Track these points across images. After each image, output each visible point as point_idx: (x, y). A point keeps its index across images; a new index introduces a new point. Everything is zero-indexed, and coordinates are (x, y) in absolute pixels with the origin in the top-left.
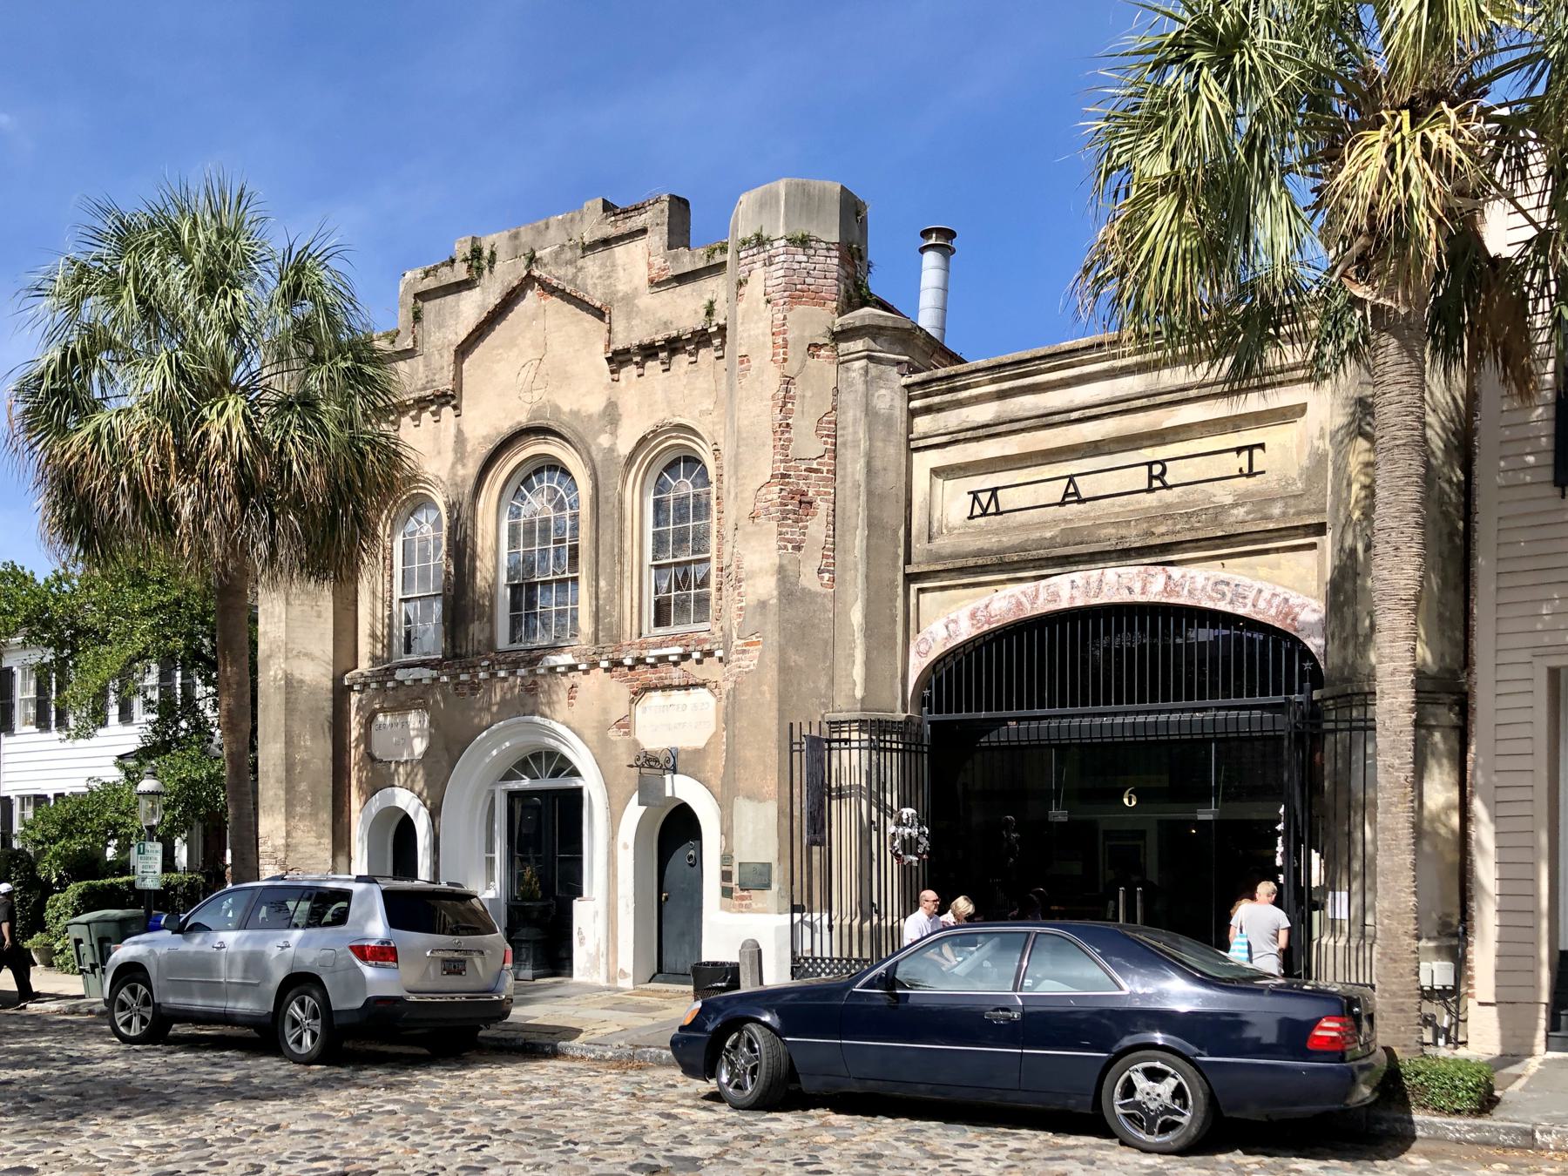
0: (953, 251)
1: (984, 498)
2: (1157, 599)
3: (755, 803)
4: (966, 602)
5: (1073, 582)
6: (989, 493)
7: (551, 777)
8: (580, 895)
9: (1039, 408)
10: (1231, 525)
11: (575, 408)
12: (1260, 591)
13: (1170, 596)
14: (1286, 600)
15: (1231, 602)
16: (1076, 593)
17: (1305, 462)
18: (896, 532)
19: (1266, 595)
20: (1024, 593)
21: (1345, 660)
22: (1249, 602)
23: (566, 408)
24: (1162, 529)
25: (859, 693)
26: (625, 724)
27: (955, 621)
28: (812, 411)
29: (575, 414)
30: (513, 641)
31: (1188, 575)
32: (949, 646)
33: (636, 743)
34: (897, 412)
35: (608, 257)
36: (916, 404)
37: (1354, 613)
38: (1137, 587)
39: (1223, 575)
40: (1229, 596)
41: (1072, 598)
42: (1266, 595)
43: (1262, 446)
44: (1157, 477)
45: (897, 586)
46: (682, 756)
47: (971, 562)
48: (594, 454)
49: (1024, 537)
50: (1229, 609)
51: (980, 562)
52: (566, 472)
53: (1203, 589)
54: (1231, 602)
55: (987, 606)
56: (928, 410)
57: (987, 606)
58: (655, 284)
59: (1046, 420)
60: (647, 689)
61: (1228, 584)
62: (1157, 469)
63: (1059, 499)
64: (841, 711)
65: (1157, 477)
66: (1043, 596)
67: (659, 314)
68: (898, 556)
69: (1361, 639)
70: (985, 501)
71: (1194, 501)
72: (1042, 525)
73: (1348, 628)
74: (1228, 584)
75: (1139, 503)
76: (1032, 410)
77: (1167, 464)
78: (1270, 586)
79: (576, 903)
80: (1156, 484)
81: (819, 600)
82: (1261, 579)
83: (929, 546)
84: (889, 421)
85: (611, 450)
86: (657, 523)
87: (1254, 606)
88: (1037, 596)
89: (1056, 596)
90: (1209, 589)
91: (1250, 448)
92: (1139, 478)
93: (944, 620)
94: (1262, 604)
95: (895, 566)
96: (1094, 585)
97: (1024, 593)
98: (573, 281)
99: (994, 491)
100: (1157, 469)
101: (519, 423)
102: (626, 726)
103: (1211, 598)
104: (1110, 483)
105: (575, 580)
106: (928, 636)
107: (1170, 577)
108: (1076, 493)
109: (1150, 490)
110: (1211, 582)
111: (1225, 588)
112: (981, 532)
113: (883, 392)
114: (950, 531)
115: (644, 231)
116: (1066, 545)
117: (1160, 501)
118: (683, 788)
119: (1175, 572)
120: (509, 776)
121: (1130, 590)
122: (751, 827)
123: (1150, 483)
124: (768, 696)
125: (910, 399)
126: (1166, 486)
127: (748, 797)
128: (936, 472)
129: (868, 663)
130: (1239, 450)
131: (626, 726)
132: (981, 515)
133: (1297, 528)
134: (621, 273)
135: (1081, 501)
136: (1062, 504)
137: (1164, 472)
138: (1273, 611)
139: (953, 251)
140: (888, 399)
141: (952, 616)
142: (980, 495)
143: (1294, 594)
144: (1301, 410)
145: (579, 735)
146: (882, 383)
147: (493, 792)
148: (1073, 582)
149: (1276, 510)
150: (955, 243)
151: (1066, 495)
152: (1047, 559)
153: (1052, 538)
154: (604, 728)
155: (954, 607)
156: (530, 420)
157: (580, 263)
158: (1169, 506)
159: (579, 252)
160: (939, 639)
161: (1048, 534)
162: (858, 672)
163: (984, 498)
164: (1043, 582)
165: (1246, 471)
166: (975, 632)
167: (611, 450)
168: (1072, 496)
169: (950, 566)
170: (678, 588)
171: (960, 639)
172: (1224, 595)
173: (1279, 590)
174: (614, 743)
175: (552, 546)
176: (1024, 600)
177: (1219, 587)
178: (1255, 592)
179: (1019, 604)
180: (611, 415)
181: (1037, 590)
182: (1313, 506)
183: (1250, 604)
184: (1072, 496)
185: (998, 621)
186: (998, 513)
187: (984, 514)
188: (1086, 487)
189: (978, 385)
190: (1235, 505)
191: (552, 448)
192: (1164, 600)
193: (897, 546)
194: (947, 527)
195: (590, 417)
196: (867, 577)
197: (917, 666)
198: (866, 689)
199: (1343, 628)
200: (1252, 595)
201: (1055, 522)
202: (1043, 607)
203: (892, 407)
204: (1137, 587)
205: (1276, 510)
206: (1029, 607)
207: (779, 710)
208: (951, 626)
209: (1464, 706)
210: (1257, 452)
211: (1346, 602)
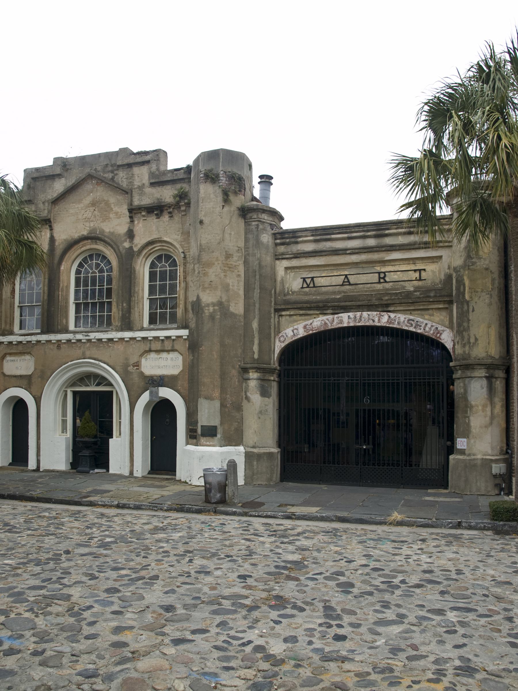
0: (272, 184)
1: (308, 281)
2: (385, 325)
3: (209, 401)
4: (301, 322)
5: (349, 316)
6: (310, 279)
7: (96, 386)
8: (112, 438)
9: (332, 248)
10: (414, 298)
11: (112, 230)
12: (426, 324)
13: (390, 324)
14: (437, 328)
15: (415, 328)
16: (350, 321)
17: (443, 277)
18: (271, 291)
19: (429, 326)
20: (327, 319)
21: (464, 352)
22: (422, 328)
23: (107, 230)
24: (386, 298)
25: (256, 356)
26: (137, 365)
27: (297, 329)
28: (234, 240)
29: (112, 233)
30: (76, 327)
31: (397, 316)
32: (294, 339)
33: (142, 373)
34: (270, 244)
35: (130, 171)
36: (278, 241)
37: (469, 335)
38: (376, 319)
39: (412, 317)
40: (414, 325)
41: (349, 322)
42: (429, 326)
43: (424, 270)
44: (382, 278)
45: (271, 314)
46: (166, 380)
47: (305, 305)
48: (121, 250)
49: (327, 297)
50: (414, 330)
51: (309, 306)
52: (104, 257)
53: (404, 321)
54: (415, 328)
55: (311, 324)
56: (282, 244)
57: (311, 324)
58: (152, 184)
59: (336, 252)
60: (150, 351)
61: (413, 321)
62: (382, 275)
63: (341, 283)
64: (248, 364)
65: (382, 278)
66: (336, 321)
67: (155, 196)
68: (271, 302)
69: (472, 344)
70: (308, 282)
71: (398, 288)
72: (334, 293)
73: (466, 340)
74: (413, 321)
75: (375, 287)
76: (329, 248)
77: (386, 273)
78: (430, 322)
79: (110, 440)
80: (382, 281)
81: (238, 317)
82: (426, 319)
83: (284, 298)
84: (267, 248)
85: (131, 248)
86: (150, 280)
87: (424, 330)
88: (333, 321)
89: (341, 322)
90: (406, 322)
91: (420, 270)
92: (375, 278)
93: (292, 328)
94: (427, 329)
95: (271, 306)
96: (358, 318)
97: (327, 319)
98: (113, 179)
99: (312, 278)
100: (382, 275)
101: (83, 235)
102: (138, 366)
103: (407, 326)
104: (363, 279)
105: (110, 303)
106: (284, 334)
107: (390, 317)
108: (348, 281)
109: (379, 282)
110: (406, 320)
111: (413, 322)
112: (306, 294)
113: (264, 235)
114: (293, 293)
115: (148, 162)
116: (345, 302)
117: (384, 287)
118: (165, 393)
119: (392, 315)
120: (73, 385)
121: (374, 321)
122: (207, 411)
123: (379, 280)
124: (216, 356)
125: (276, 239)
126: (386, 282)
127: (206, 398)
128: (287, 268)
129: (260, 344)
130: (415, 271)
131: (138, 366)
132: (307, 287)
133: (441, 301)
134: (136, 177)
135: (350, 284)
136: (342, 285)
137: (385, 276)
138: (432, 332)
139: (272, 184)
140: (267, 238)
141: (295, 327)
142: (306, 279)
143: (440, 326)
144: (440, 257)
145: (113, 369)
146: (264, 232)
147: (66, 391)
148: (349, 316)
149: (432, 294)
150: (272, 181)
151: (344, 282)
152: (338, 306)
153: (339, 298)
154: (126, 366)
155: (296, 324)
156: (88, 234)
157: (115, 172)
158: (388, 289)
159: (115, 168)
160: (289, 336)
161: (338, 297)
162: (256, 348)
163: (308, 281)
164: (336, 316)
165: (418, 278)
166: (305, 334)
167: (131, 248)
168: (347, 282)
169: (295, 307)
170: (161, 308)
171: (299, 336)
172: (412, 325)
173: (434, 324)
174: (132, 373)
175: (97, 287)
176: (327, 322)
177: (410, 322)
178: (424, 324)
179: (326, 323)
180: (131, 235)
181: (333, 319)
182: (446, 294)
183: (422, 329)
184: (347, 282)
185: (316, 330)
186: (314, 287)
187: (308, 287)
188: (352, 279)
189: (306, 236)
190: (415, 291)
191: (100, 247)
192: (387, 325)
193: (271, 297)
194: (291, 291)
195: (119, 235)
196: (259, 309)
197: (278, 346)
198: (259, 355)
199: (463, 340)
200: (423, 325)
201: (339, 292)
202: (336, 325)
203: (268, 242)
204: (376, 319)
205: (432, 294)
206: (330, 325)
207: (221, 362)
208: (295, 331)
209: (508, 371)
210: (422, 272)
211: (464, 330)
